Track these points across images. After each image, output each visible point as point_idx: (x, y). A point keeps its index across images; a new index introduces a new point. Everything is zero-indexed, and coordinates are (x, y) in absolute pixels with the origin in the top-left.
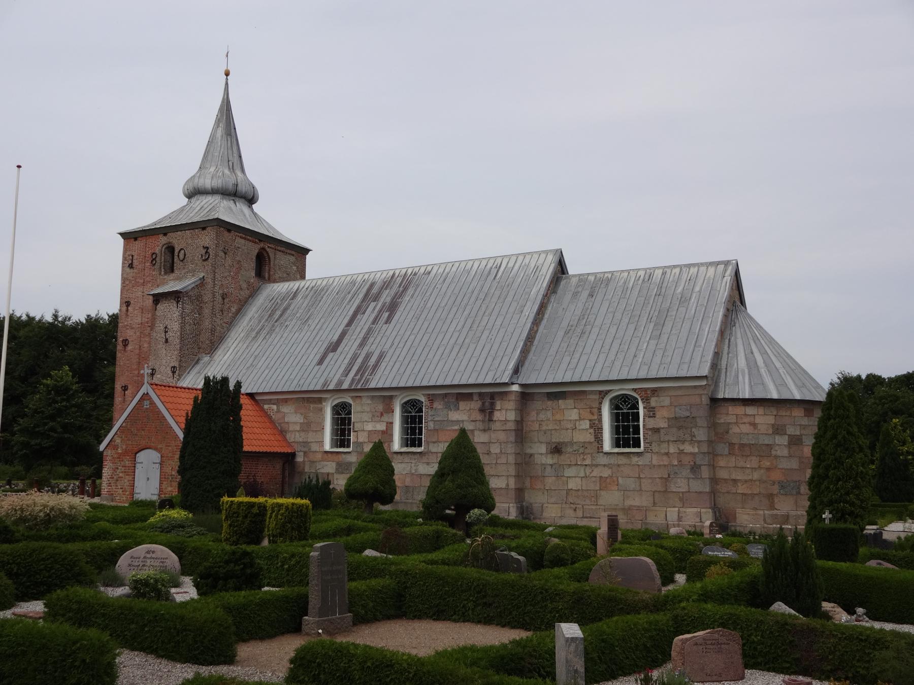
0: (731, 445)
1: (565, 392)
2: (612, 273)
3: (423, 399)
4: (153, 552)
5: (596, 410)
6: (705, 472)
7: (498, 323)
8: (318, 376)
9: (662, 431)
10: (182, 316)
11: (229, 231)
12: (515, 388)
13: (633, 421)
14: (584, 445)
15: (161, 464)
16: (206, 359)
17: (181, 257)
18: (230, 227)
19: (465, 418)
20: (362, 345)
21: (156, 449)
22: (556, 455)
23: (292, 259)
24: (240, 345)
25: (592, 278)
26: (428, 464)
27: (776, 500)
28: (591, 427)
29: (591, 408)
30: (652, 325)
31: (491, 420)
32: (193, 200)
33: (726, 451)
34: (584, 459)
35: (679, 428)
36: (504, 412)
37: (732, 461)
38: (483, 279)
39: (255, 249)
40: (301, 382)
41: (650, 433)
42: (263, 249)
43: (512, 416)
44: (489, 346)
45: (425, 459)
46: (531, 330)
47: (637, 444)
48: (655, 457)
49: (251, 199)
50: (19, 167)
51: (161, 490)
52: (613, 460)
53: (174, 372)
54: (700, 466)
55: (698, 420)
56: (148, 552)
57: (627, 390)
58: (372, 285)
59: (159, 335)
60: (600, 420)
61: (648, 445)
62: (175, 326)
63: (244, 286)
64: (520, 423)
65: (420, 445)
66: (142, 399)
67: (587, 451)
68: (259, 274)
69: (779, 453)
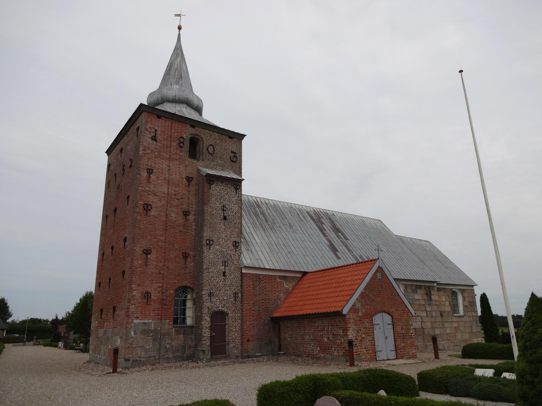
15: (393, 324)
19: (420, 298)
24: (258, 233)
31: (431, 300)
50: (461, 71)
66: (377, 271)
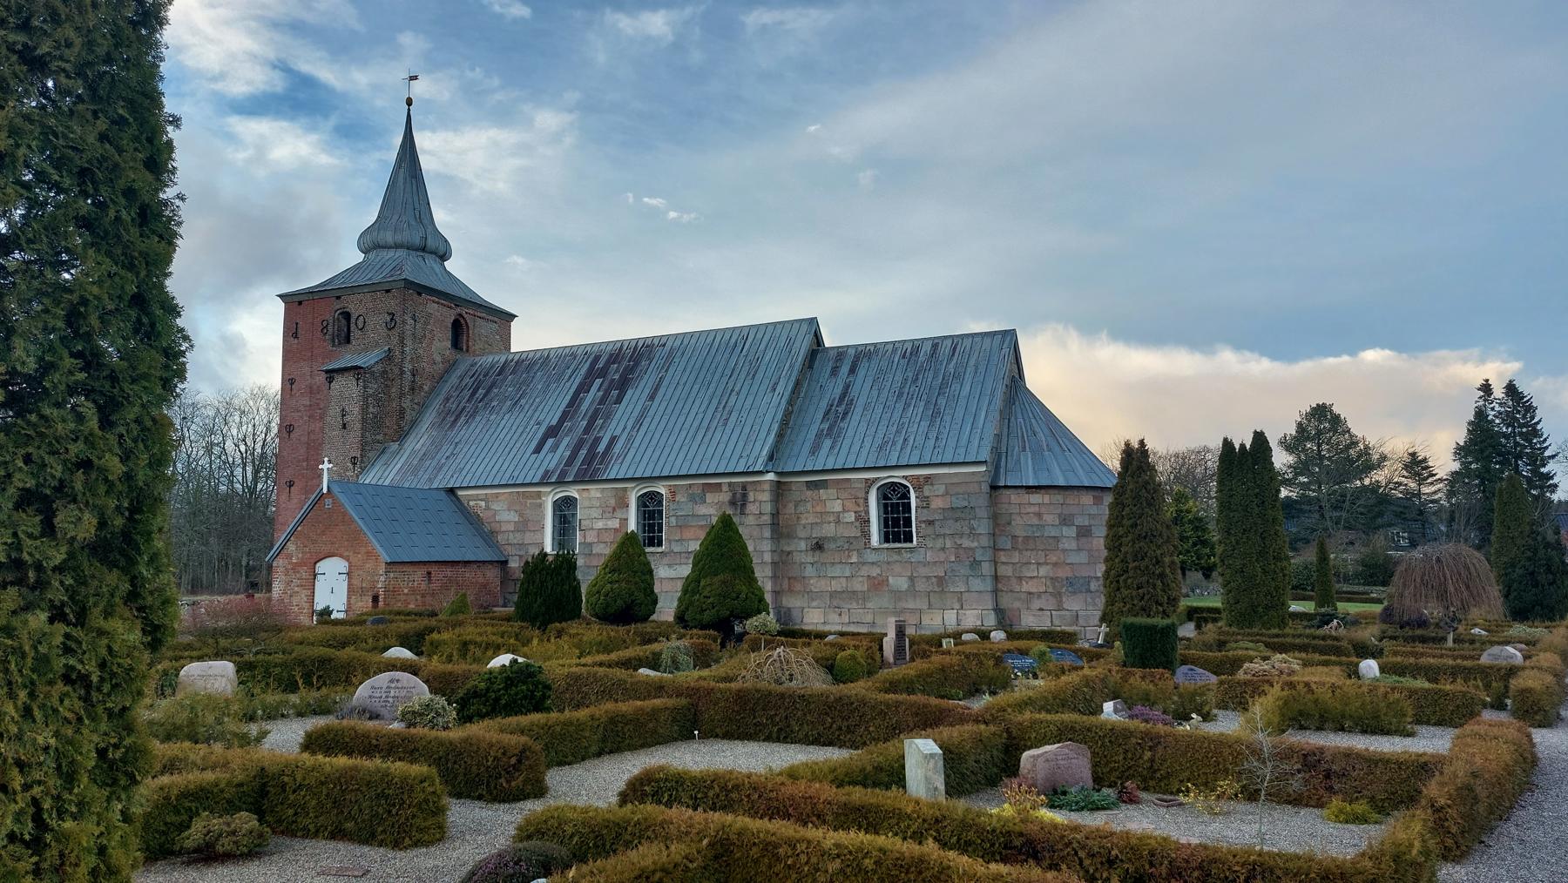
0: (1014, 537)
2: (875, 345)
6: (986, 568)
7: (749, 401)
10: (365, 398)
11: (420, 294)
12: (771, 476)
14: (849, 540)
16: (395, 446)
18: (421, 289)
20: (587, 430)
21: (341, 556)
32: (372, 255)
35: (957, 520)
37: (1016, 557)
43: (768, 508)
45: (666, 560)
49: (444, 256)
52: (883, 557)
57: (898, 476)
58: (597, 358)
60: (867, 512)
62: (355, 411)
63: (438, 359)
64: (775, 515)
65: (660, 544)
69: (1066, 546)
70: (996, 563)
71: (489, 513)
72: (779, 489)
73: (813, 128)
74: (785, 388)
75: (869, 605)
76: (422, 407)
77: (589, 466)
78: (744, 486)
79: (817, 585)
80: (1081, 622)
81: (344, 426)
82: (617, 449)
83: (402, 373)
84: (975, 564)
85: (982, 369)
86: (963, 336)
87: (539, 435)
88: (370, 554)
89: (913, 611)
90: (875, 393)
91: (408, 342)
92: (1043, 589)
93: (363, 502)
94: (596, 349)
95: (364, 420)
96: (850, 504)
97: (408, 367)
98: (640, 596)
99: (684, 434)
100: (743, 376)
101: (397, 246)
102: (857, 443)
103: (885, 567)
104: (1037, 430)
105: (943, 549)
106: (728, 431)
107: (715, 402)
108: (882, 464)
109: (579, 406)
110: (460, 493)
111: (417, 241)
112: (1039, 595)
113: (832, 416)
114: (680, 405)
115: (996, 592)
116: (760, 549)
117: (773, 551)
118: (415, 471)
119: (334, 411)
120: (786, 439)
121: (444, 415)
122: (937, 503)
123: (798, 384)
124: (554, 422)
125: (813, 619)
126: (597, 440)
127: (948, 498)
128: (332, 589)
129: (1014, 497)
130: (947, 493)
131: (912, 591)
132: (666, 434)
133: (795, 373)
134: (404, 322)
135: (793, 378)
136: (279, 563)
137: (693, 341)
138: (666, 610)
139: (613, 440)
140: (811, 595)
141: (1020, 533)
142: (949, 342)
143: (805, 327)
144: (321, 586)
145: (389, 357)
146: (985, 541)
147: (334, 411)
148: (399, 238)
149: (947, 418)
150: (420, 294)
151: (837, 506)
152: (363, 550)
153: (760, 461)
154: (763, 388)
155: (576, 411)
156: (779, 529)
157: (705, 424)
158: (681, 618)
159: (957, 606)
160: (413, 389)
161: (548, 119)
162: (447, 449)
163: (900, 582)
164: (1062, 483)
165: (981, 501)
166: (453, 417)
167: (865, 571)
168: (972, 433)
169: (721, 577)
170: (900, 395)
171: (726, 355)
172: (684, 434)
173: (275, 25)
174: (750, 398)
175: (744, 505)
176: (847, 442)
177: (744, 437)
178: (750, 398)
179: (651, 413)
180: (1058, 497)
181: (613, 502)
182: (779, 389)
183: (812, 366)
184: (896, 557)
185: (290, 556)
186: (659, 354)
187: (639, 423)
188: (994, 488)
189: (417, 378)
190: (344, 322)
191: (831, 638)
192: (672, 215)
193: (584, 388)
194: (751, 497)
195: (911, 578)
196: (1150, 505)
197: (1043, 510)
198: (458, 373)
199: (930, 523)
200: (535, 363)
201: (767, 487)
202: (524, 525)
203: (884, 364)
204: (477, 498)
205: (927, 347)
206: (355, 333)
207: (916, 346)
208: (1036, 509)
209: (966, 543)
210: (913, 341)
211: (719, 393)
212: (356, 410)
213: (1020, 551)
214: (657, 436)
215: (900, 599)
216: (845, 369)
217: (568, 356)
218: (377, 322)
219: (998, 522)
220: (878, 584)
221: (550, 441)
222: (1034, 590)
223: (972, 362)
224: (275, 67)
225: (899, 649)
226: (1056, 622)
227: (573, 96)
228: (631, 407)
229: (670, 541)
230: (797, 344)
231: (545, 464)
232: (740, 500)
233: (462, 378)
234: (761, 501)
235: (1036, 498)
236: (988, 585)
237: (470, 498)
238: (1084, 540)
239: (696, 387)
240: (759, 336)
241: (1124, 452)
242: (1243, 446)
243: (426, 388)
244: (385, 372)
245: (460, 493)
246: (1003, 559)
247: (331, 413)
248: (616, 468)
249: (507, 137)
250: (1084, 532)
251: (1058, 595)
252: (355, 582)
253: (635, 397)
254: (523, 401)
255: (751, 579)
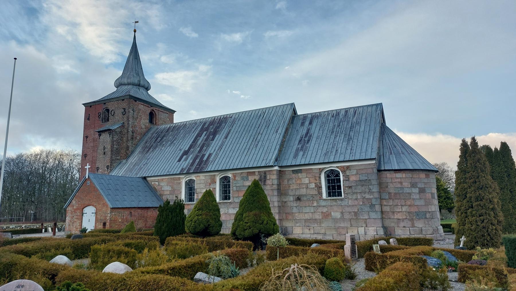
0: (390, 193)
1: (301, 169)
2: (320, 113)
3: (230, 176)
4: (23, 286)
5: (318, 178)
6: (378, 208)
7: (266, 137)
8: (178, 167)
9: (353, 187)
10: (113, 142)
11: (136, 101)
12: (276, 168)
13: (337, 183)
14: (312, 196)
16: (124, 161)
17: (113, 114)
18: (136, 99)
20: (200, 152)
21: (93, 206)
22: (298, 202)
23: (167, 115)
25: (310, 116)
26: (233, 208)
27: (415, 222)
28: (316, 186)
29: (315, 177)
30: (343, 135)
32: (119, 88)
33: (387, 197)
34: (313, 203)
35: (362, 186)
36: (271, 180)
37: (391, 203)
38: (258, 118)
39: (148, 110)
40: (170, 170)
41: (347, 189)
42: (153, 110)
43: (276, 182)
44: (262, 148)
45: (232, 206)
46: (282, 140)
47: (340, 194)
48: (350, 201)
49: (147, 89)
50: (15, 59)
51: (96, 226)
52: (329, 203)
53: (108, 168)
54: (375, 205)
55: (372, 181)
56: (18, 287)
57: (334, 167)
58: (205, 124)
59: (100, 150)
60: (320, 183)
61: (346, 195)
62: (109, 147)
63: (143, 127)
64: (279, 185)
65: (229, 199)
67: (314, 199)
68: (151, 121)
69: (414, 197)
70: (381, 205)
71: (160, 187)
72: (280, 174)
73: (287, 68)
74: (282, 131)
75: (323, 225)
76: (136, 145)
77: (199, 166)
78: (265, 173)
79: (298, 216)
80: (424, 233)
81: (104, 154)
82: (211, 159)
83: (128, 132)
84: (372, 206)
85: (369, 119)
86: (358, 107)
87: (180, 155)
88: (105, 205)
89: (343, 228)
90: (321, 132)
91: (131, 120)
92: (405, 217)
93: (103, 182)
94: (204, 120)
95: (112, 151)
96: (312, 180)
97: (130, 129)
98: (212, 222)
99: (239, 151)
100: (263, 127)
101: (129, 84)
102: (314, 153)
103: (329, 208)
104: (396, 145)
105: (356, 199)
106: (258, 149)
107: (252, 138)
108: (327, 161)
109: (197, 143)
110: (148, 179)
111: (136, 81)
112: (403, 220)
113: (302, 142)
114: (238, 139)
115: (382, 218)
116: (273, 201)
117: (278, 201)
118: (131, 170)
119: (101, 147)
120: (283, 152)
121: (144, 148)
122: (353, 178)
123: (287, 130)
124: (187, 149)
125: (299, 232)
126: (204, 155)
127: (358, 176)
128: (89, 221)
129: (389, 175)
130: (357, 174)
131: (343, 219)
132: (232, 152)
133: (286, 125)
134: (129, 112)
135: (285, 127)
136: (69, 209)
137: (243, 115)
138: (227, 229)
139: (210, 155)
140: (297, 221)
141: (392, 191)
142: (353, 110)
143: (289, 107)
144: (85, 218)
145: (123, 126)
146: (376, 195)
147: (101, 147)
148: (129, 81)
149: (355, 141)
150: (136, 101)
151: (306, 181)
152: (102, 203)
153: (272, 161)
154: (272, 131)
155: (195, 144)
156: (281, 192)
157: (248, 147)
158: (234, 234)
159: (364, 225)
160: (132, 138)
161: (203, 68)
162: (144, 161)
163: (337, 215)
164: (411, 168)
165: (374, 177)
166: (147, 149)
167: (320, 210)
168: (367, 147)
169: (253, 212)
170: (333, 132)
171: (257, 120)
172: (239, 151)
173: (119, 42)
174: (267, 136)
175: (265, 181)
176: (310, 152)
177: (264, 151)
178: (267, 136)
179: (226, 144)
180: (409, 175)
181: (209, 181)
182: (279, 131)
183: (293, 123)
184: (335, 203)
185: (73, 206)
186: (230, 121)
187: (220, 148)
188: (379, 171)
189: (134, 134)
190: (107, 113)
191: (314, 246)
192: (242, 96)
193: (199, 135)
194: (268, 177)
195: (342, 213)
196: (482, 171)
197: (402, 180)
198: (151, 132)
199: (350, 187)
200: (181, 127)
201: (275, 172)
202: (173, 192)
203: (324, 120)
204: (155, 181)
205: (343, 112)
206: (111, 117)
207: (337, 113)
208: (399, 180)
209: (367, 196)
210: (336, 110)
211: (253, 134)
212: (109, 147)
213: (393, 200)
214: (228, 153)
215: (337, 222)
216: (307, 123)
217: (194, 124)
218: (119, 113)
219: (381, 185)
220: (326, 216)
221: (185, 157)
222: (401, 218)
223: (364, 117)
224: (118, 55)
225: (353, 252)
226: (412, 233)
227: (211, 60)
228: (218, 141)
229: (233, 197)
230: (286, 113)
231: (182, 166)
232: (264, 178)
233: (152, 134)
234: (272, 179)
235: (399, 175)
236: (379, 216)
237: (152, 181)
238: (422, 194)
239: (244, 132)
240: (270, 111)
241: (462, 144)
242: (496, 149)
243: (138, 138)
244: (121, 132)
245: (148, 179)
246: (385, 203)
247: (100, 148)
248: (211, 166)
249: (190, 74)
250: (422, 191)
251: (412, 220)
252: (98, 217)
253: (219, 138)
254: (175, 142)
255: (270, 214)
